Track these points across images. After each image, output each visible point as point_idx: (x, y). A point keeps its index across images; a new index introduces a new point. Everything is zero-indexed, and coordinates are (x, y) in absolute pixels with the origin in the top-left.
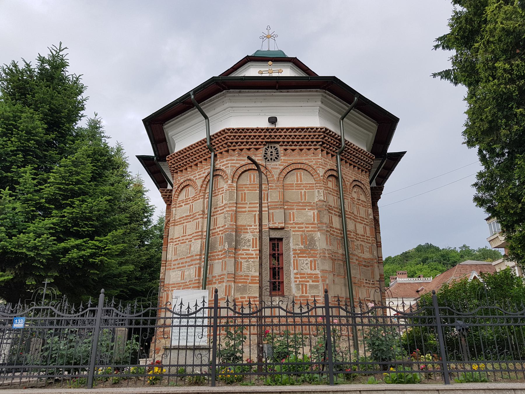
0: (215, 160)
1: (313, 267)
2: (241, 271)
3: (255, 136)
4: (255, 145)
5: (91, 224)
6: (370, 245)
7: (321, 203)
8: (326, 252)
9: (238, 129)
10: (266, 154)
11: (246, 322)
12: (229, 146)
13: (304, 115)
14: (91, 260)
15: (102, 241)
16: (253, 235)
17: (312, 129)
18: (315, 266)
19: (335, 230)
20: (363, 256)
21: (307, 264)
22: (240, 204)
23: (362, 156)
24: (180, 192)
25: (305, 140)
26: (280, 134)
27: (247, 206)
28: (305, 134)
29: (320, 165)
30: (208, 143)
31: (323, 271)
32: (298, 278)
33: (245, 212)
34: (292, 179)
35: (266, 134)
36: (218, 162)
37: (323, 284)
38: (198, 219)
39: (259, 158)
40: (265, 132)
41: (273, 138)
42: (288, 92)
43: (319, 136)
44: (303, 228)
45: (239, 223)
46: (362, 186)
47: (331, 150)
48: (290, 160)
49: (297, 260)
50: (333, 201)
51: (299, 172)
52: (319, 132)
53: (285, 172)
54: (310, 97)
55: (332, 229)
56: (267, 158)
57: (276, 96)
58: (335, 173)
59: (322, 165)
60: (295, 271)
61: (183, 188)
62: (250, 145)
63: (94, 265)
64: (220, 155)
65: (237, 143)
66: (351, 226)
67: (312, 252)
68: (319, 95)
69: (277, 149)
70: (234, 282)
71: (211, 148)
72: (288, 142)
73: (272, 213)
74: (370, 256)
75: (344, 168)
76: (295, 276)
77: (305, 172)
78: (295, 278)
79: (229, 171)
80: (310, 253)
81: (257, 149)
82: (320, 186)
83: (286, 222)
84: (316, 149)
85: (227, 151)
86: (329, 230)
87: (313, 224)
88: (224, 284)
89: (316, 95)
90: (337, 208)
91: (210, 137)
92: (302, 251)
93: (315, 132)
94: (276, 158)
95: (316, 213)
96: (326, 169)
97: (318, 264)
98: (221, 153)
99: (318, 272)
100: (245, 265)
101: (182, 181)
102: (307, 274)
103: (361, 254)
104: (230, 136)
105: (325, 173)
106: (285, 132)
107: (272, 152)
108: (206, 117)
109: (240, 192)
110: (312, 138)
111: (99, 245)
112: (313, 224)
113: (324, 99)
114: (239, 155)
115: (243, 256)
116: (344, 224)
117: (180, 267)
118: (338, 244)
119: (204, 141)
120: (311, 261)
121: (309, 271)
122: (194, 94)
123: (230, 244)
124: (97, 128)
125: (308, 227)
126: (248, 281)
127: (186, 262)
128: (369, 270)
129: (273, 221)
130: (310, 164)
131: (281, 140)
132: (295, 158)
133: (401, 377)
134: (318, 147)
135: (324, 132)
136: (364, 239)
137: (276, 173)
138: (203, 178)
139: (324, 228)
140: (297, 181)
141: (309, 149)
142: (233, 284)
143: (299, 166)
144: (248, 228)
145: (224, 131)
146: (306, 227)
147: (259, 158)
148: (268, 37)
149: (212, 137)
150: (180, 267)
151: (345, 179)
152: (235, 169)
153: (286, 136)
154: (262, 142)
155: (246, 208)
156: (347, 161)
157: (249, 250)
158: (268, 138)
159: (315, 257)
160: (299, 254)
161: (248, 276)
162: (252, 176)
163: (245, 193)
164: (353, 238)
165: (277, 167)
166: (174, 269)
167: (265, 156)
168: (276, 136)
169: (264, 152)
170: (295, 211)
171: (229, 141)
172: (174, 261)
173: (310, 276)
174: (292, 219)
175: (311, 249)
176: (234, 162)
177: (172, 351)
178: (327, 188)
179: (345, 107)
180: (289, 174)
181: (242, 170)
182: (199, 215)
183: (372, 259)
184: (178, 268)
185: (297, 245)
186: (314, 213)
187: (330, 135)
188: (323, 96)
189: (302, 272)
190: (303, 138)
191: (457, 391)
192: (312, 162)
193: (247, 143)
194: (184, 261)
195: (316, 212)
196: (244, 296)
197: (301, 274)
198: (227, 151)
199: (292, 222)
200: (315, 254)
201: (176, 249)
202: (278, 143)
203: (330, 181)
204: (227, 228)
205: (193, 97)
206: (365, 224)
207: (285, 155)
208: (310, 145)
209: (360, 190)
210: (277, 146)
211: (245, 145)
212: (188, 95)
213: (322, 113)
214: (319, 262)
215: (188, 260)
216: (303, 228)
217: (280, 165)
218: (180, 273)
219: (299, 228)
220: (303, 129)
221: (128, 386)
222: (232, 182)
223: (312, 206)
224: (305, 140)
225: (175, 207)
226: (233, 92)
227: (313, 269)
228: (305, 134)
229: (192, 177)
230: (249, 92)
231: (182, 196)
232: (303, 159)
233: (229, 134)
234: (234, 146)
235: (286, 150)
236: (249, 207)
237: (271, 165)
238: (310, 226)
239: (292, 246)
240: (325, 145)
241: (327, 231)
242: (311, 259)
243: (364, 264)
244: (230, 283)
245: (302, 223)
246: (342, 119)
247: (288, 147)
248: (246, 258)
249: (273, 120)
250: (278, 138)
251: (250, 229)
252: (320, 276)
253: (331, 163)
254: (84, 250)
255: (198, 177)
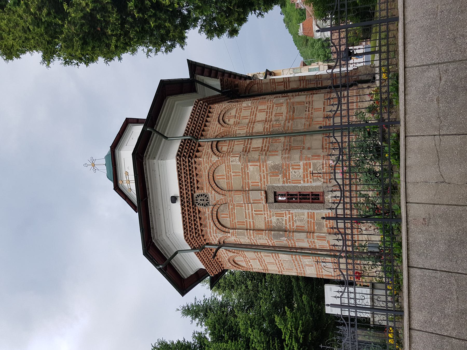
0: (211, 244)
1: (297, 167)
2: (304, 227)
3: (189, 215)
4: (196, 214)
5: (272, 341)
6: (275, 105)
7: (242, 159)
8: (284, 156)
9: (184, 229)
10: (203, 204)
11: (346, 188)
12: (199, 235)
13: (167, 173)
14: (301, 342)
15: (285, 333)
16: (273, 216)
17: (178, 167)
18: (297, 165)
19: (264, 144)
20: (284, 114)
21: (295, 172)
22: (247, 226)
23: (197, 115)
24: (239, 265)
25: (188, 173)
26: (185, 194)
27: (248, 220)
28: (183, 173)
29: (208, 160)
30: (198, 251)
31: (301, 159)
32: (308, 180)
33: (253, 222)
34: (223, 183)
35: (186, 206)
36: (213, 242)
37: (312, 159)
38: (261, 256)
39: (207, 210)
40: (185, 207)
41: (189, 199)
42: (148, 189)
43: (183, 160)
44: (264, 175)
45: (263, 227)
46: (223, 112)
47: (195, 148)
48: (207, 185)
49: (292, 181)
50: (239, 147)
51: (216, 178)
52: (180, 161)
53: (217, 189)
54: (151, 170)
55: (264, 148)
56: (206, 204)
57: (153, 199)
58: (215, 144)
59: (209, 158)
60: (302, 182)
61: (236, 263)
62: (196, 218)
63: (305, 338)
64: (206, 240)
65: (196, 229)
66: (259, 128)
67: (284, 167)
68: (149, 162)
69: (198, 196)
70: (313, 233)
71: (202, 248)
72: (191, 186)
73: (253, 200)
74: (285, 105)
75: (209, 132)
76: (306, 183)
77: (215, 171)
78: (308, 182)
79: (220, 235)
80: (285, 169)
81: (199, 212)
82: (227, 160)
83: (260, 189)
84: (195, 162)
85: (203, 236)
86: (264, 152)
87: (260, 166)
88: (316, 241)
89: (149, 165)
90: (245, 142)
91: (192, 249)
92: (285, 176)
93: (180, 165)
94: (206, 196)
95: (251, 164)
96: (212, 153)
97: (294, 163)
98: (205, 240)
99: (301, 163)
100: (298, 224)
101: (230, 265)
102: (304, 172)
103: (284, 116)
104: (191, 235)
105: (215, 154)
106: (183, 190)
107: (201, 200)
108: (176, 253)
109: (237, 226)
110: (186, 166)
111: (288, 334)
112: (260, 166)
113: (151, 157)
114: (205, 226)
115: (291, 225)
116: (259, 135)
117: (303, 267)
118: (276, 142)
119: (197, 254)
120: (293, 169)
121: (301, 171)
122: (158, 265)
123: (282, 236)
124: (188, 309)
125: (263, 170)
126: (312, 221)
127: (298, 263)
128: (297, 107)
129: (260, 200)
130: (208, 168)
131: (190, 193)
132: (204, 180)
133: (394, 154)
134: (193, 161)
135: (180, 157)
136: (269, 112)
137: (219, 197)
138: (227, 252)
139: (263, 157)
140: (224, 179)
141: (196, 168)
142: (315, 234)
143: (211, 177)
144: (267, 220)
145: (186, 240)
146: (264, 172)
147: (207, 210)
148: (94, 165)
149: (193, 248)
150: (303, 267)
151: (219, 132)
152: (218, 231)
153: (186, 189)
154: (193, 208)
155: (250, 222)
156: (202, 129)
157: (286, 220)
158: (190, 204)
159: (289, 165)
160: (287, 178)
161: (308, 221)
162: (223, 216)
163: (238, 222)
164: (270, 125)
165: (213, 196)
166: (304, 271)
167: (205, 206)
168: (187, 197)
169: (201, 206)
170: (250, 181)
171: (194, 235)
172: (297, 270)
173: (305, 170)
174: (257, 184)
175: (282, 168)
176: (212, 231)
177: (374, 293)
178: (229, 153)
179: (155, 136)
180: (218, 185)
181: (218, 225)
182: (258, 255)
183: (287, 103)
184: (303, 268)
185: (279, 180)
186: (251, 165)
187: (182, 150)
188: (148, 159)
189: (302, 176)
190: (187, 175)
191: (406, 120)
192: (206, 166)
193: (195, 220)
194: (297, 264)
195: (249, 164)
196: (325, 224)
197: (304, 177)
198: (203, 236)
199: (260, 184)
200: (286, 165)
201: (287, 269)
202: (192, 195)
203: (222, 148)
204: (269, 238)
205: (161, 266)
206: (256, 111)
207: (202, 189)
208: (192, 168)
209: (227, 115)
210: (195, 195)
211: (197, 222)
212: (160, 270)
213: (164, 158)
214: (292, 162)
215: (296, 262)
216: (264, 175)
217: (211, 193)
218: (307, 267)
219: (264, 178)
220: (179, 175)
221: (403, 334)
222: (229, 233)
223: (245, 167)
224: (188, 173)
225: (252, 269)
226: (154, 234)
227: (299, 167)
228: (183, 173)
229: (226, 259)
230: (152, 221)
231: (243, 264)
232: (204, 174)
233: (189, 236)
234: (198, 231)
235: (198, 188)
236: (249, 219)
237: (212, 201)
238: (262, 169)
239: (280, 184)
240: (191, 154)
241: (266, 154)
242: (290, 169)
243: (292, 113)
244: (315, 237)
245: (260, 175)
246: (166, 138)
247: (196, 186)
248: (293, 223)
249: (174, 199)
250: (189, 195)
251: (268, 219)
252: (305, 162)
253: (206, 148)
254: (293, 347)
255: (226, 255)
